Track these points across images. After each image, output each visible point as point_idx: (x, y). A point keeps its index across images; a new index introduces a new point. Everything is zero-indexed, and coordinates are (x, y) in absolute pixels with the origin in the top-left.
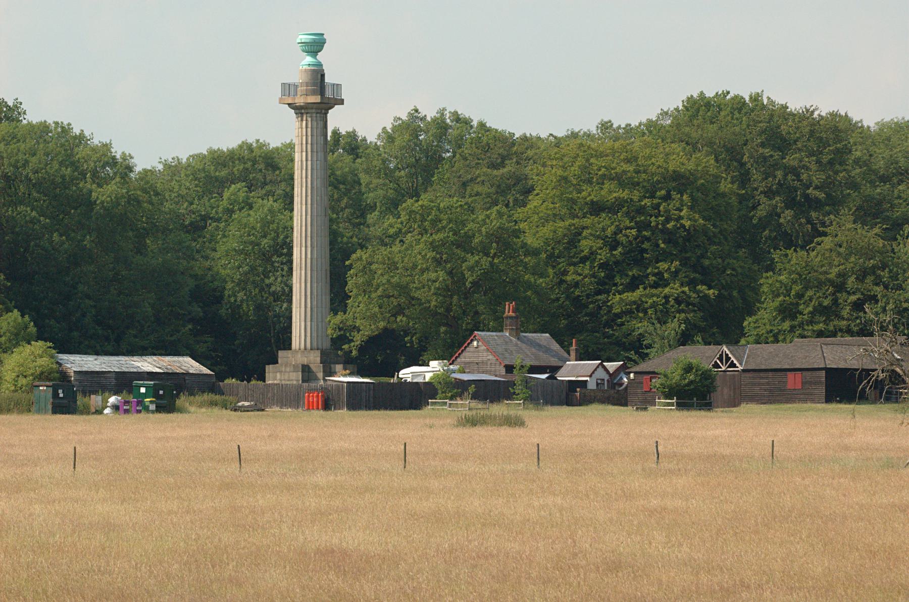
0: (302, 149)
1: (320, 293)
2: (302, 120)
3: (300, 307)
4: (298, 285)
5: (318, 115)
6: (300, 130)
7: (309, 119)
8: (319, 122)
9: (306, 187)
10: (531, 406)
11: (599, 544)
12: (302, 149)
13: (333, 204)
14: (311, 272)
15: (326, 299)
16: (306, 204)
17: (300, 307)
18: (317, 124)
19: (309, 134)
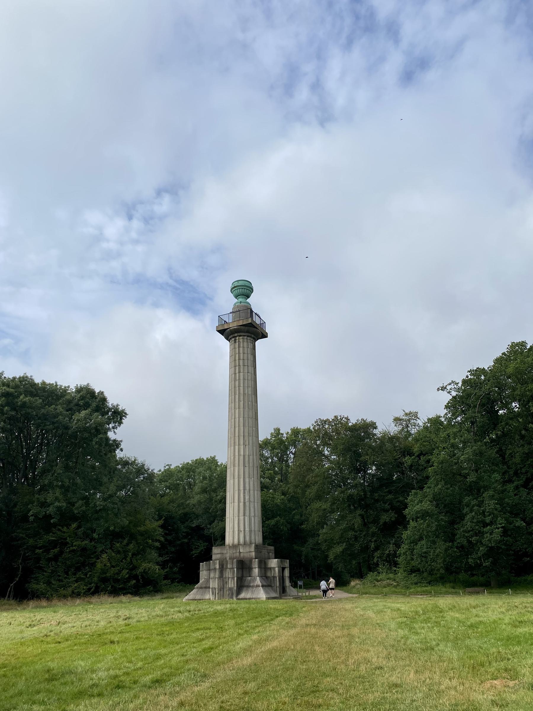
0: (235, 371)
1: (252, 488)
2: (235, 342)
3: (234, 478)
4: (232, 482)
5: (249, 338)
6: (233, 375)
7: (241, 340)
8: (249, 344)
9: (239, 490)
10: (59, 604)
11: (6, 697)
12: (235, 371)
13: (342, 641)
14: (239, 403)
15: (257, 494)
16: (239, 466)
17: (234, 478)
18: (248, 345)
19: (242, 424)
